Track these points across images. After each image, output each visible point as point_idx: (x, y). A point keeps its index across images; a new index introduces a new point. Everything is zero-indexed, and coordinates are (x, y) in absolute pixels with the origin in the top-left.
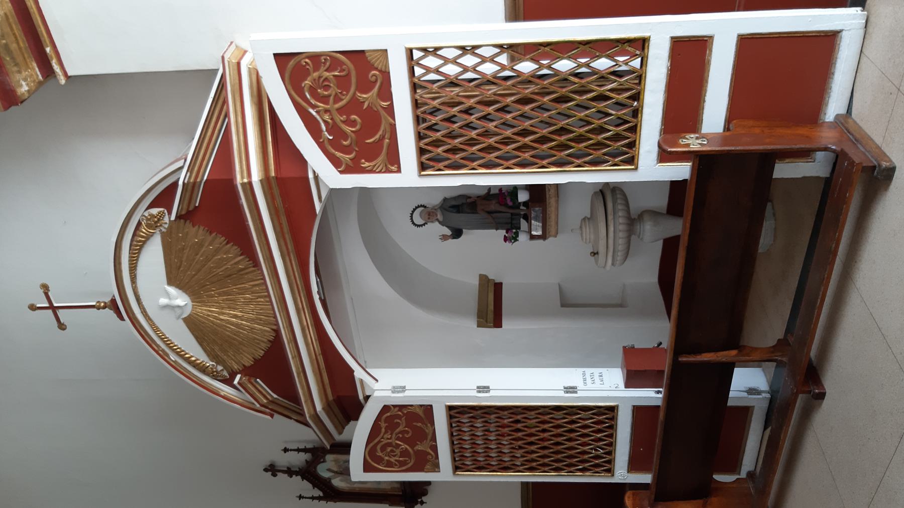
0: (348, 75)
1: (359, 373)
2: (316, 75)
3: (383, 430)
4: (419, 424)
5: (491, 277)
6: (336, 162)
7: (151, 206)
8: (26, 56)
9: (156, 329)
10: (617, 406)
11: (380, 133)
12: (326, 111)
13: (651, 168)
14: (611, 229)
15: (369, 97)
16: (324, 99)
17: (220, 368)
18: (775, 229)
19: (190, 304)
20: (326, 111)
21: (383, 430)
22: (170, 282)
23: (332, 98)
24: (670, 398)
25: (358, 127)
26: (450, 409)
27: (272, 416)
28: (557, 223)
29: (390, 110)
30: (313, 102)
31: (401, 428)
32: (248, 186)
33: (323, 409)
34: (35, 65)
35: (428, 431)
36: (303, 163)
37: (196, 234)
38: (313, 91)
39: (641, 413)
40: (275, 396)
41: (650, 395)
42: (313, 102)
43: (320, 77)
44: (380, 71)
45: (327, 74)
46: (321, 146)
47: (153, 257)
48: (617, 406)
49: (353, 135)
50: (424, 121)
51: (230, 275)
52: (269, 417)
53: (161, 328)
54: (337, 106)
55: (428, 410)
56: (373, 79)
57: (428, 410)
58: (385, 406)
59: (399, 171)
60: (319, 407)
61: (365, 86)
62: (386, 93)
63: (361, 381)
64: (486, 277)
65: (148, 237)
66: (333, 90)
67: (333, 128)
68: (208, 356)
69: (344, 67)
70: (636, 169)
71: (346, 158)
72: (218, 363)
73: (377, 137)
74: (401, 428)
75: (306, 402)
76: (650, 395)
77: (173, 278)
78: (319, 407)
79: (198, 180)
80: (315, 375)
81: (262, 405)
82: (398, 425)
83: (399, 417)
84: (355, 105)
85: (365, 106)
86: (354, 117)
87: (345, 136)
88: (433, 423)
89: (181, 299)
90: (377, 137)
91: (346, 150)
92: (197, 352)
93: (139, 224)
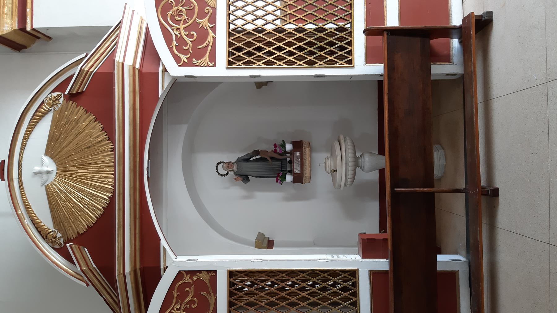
0: (194, 8)
1: (163, 243)
2: (176, 8)
3: (174, 301)
4: (204, 293)
5: (266, 236)
6: (177, 59)
7: (54, 91)
8: (14, 14)
9: (23, 195)
10: (358, 269)
11: (207, 42)
12: (178, 29)
13: (363, 66)
14: (343, 149)
15: (205, 22)
16: (178, 22)
17: (59, 235)
18: (445, 155)
19: (55, 171)
20: (178, 29)
21: (174, 301)
22: (47, 154)
23: (182, 22)
24: (394, 264)
25: (194, 38)
26: (231, 274)
27: (88, 285)
28: (310, 167)
29: (214, 29)
30: (171, 23)
31: (189, 298)
32: (121, 65)
33: (130, 272)
34: (17, 19)
35: (212, 302)
36: (158, 59)
37: (78, 112)
38: (172, 17)
39: (374, 275)
40: (95, 266)
41: (382, 264)
42: (171, 23)
43: (177, 10)
44: (211, 7)
45: (181, 8)
46: (171, 49)
47: (44, 128)
48: (358, 269)
49: (190, 43)
50: (233, 54)
51: (89, 147)
52: (84, 284)
53: (27, 195)
54: (185, 26)
55: (213, 274)
56: (207, 11)
57: (213, 274)
58: (180, 271)
59: (215, 66)
60: (128, 269)
61: (202, 15)
62: (213, 19)
63: (165, 249)
64: (263, 234)
65: (45, 114)
66: (185, 16)
67: (180, 40)
68: (54, 222)
69: (192, 5)
70: (353, 67)
71: (184, 58)
72: (59, 230)
73: (205, 44)
74: (189, 298)
75: (119, 257)
76: (382, 264)
77: (50, 151)
78: (128, 269)
79: (91, 70)
80: (131, 261)
81: (82, 270)
82: (188, 293)
83: (188, 285)
84: (195, 26)
85: (200, 26)
86: (192, 33)
87: (186, 44)
88: (215, 293)
89: (50, 165)
90: (205, 44)
91: (185, 52)
92: (47, 222)
93: (43, 102)
